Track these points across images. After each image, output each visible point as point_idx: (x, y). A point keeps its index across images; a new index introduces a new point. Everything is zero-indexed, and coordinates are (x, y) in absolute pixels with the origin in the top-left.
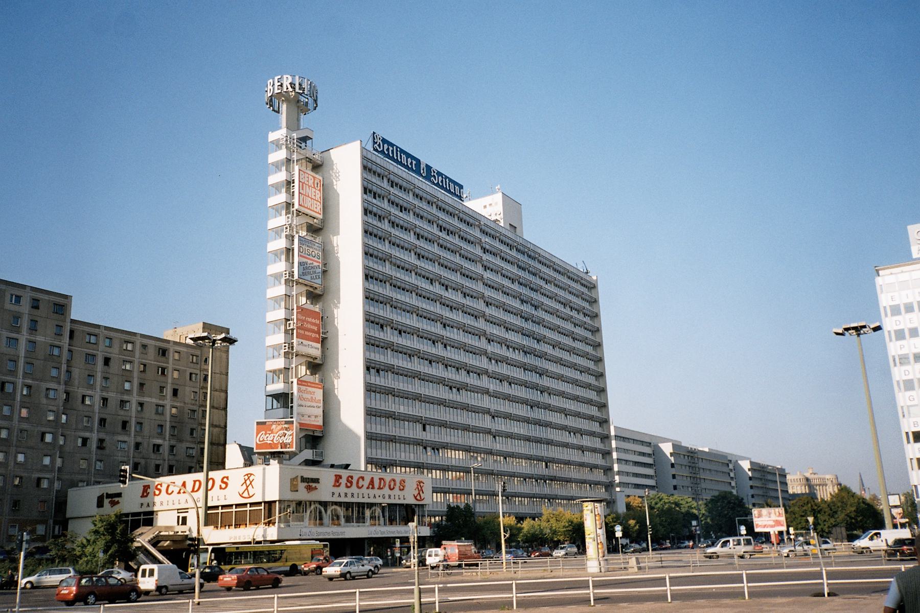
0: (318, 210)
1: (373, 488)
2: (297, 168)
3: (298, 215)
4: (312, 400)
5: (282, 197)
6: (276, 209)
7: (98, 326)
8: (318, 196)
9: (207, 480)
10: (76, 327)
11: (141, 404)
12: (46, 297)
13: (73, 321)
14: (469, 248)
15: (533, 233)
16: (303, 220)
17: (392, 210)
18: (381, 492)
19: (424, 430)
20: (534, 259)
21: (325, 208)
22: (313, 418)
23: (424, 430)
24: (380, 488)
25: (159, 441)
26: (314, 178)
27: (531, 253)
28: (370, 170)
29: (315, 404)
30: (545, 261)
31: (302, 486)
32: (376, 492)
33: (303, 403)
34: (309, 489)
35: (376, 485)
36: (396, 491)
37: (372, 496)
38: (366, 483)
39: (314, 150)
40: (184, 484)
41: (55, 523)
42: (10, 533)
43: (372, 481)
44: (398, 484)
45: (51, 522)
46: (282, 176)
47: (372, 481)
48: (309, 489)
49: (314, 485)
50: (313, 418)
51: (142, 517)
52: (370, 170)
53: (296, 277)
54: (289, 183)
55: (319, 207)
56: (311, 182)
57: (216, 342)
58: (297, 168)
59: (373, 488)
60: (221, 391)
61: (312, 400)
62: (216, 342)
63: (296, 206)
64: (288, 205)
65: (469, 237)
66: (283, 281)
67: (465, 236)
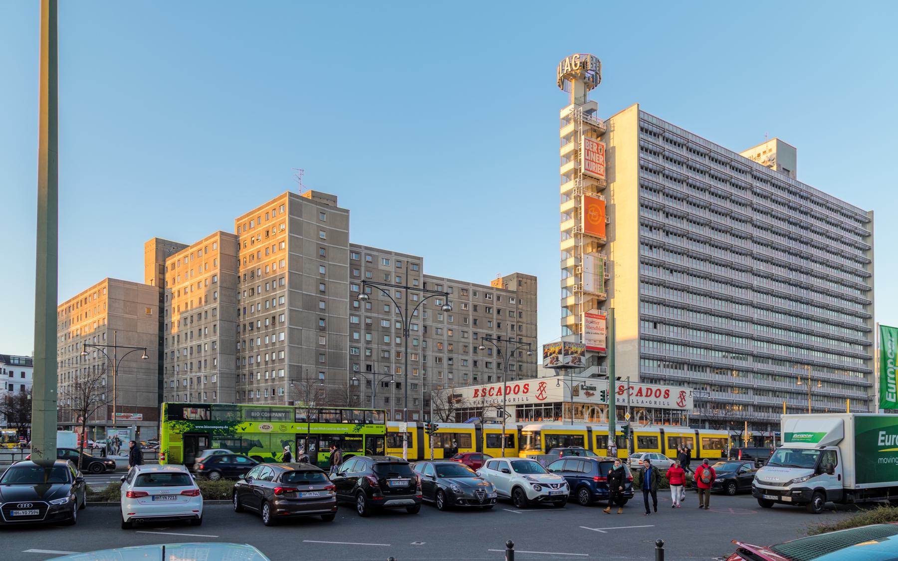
0: (601, 172)
1: (641, 395)
2: (583, 137)
3: (584, 179)
4: (597, 328)
5: (570, 166)
6: (567, 175)
7: (443, 279)
8: (601, 161)
9: (506, 388)
10: (427, 280)
11: (476, 334)
12: (481, 289)
13: (425, 276)
14: (741, 177)
15: (807, 175)
16: (589, 183)
17: (667, 165)
18: (648, 399)
19: (655, 327)
20: (806, 198)
21: (607, 170)
22: (598, 343)
23: (655, 327)
24: (647, 396)
25: (489, 360)
26: (598, 144)
27: (805, 195)
28: (646, 131)
29: (599, 332)
30: (817, 200)
31: (582, 392)
32: (644, 398)
33: (590, 331)
34: (588, 394)
35: (644, 393)
36: (662, 399)
37: (640, 401)
38: (635, 391)
39: (598, 119)
40: (500, 389)
41: (424, 413)
42: (620, 403)
43: (640, 390)
44: (663, 393)
45: (422, 412)
46: (570, 147)
47: (640, 390)
48: (588, 394)
49: (591, 392)
50: (592, 342)
51: (543, 407)
52: (646, 131)
53: (583, 231)
54: (576, 152)
55: (602, 170)
56: (595, 149)
57: (524, 288)
58: (583, 137)
59: (641, 395)
60: (531, 324)
61: (597, 328)
62: (524, 288)
63: (583, 171)
64: (576, 171)
65: (740, 183)
66: (572, 235)
67: (736, 182)
